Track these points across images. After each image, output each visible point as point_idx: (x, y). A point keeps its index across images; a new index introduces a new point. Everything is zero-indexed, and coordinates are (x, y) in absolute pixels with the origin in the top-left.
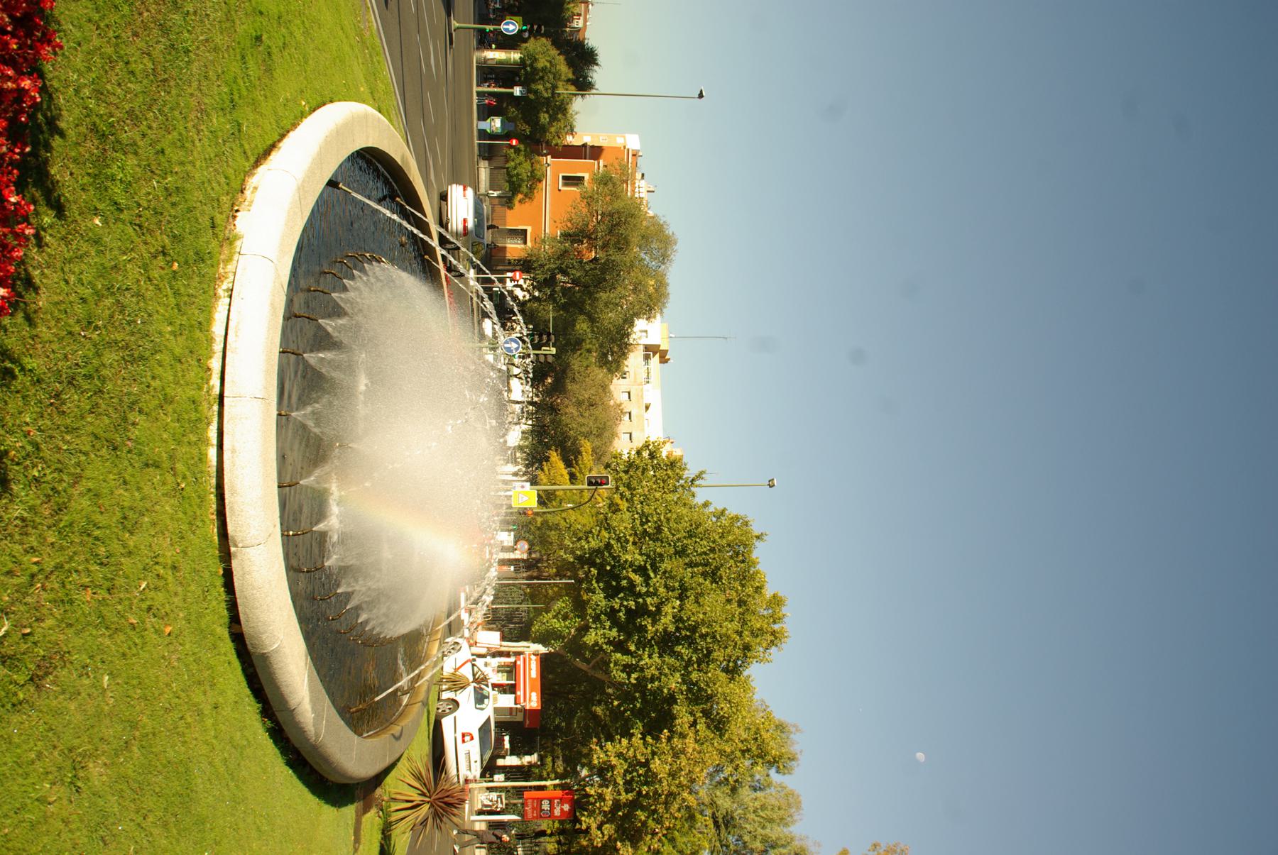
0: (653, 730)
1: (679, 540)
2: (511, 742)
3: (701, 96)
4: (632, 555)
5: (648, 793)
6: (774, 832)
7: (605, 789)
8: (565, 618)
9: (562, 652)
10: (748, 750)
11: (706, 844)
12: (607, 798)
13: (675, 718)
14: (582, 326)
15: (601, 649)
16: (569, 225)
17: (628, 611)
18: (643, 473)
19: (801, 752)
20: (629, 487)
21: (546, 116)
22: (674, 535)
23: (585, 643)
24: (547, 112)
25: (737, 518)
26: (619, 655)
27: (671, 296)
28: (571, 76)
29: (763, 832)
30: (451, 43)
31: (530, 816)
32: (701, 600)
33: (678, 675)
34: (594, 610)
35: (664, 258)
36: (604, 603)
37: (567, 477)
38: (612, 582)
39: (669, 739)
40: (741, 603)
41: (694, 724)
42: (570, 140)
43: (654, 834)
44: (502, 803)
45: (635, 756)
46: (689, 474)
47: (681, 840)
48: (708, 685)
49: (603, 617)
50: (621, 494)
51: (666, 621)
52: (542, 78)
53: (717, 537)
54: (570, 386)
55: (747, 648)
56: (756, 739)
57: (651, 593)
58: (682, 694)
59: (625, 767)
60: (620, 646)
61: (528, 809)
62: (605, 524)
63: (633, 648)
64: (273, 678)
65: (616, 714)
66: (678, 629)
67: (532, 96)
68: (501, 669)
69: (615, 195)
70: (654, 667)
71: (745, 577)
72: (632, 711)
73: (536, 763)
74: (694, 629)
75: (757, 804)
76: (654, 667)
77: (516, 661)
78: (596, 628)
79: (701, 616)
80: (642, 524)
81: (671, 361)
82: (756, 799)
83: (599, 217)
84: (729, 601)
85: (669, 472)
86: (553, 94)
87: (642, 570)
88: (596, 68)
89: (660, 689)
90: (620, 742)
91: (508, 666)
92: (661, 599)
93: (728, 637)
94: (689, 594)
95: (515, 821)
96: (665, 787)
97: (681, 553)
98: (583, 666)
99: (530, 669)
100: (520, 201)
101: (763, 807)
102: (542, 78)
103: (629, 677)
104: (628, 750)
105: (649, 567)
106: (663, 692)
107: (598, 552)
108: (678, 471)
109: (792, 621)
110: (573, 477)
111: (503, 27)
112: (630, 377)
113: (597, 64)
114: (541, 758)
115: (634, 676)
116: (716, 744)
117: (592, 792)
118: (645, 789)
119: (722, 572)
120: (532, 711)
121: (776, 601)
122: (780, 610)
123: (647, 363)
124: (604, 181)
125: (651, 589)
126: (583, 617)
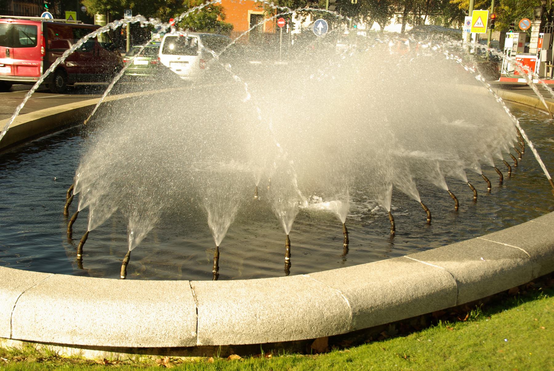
64: (398, 306)
100: (223, 19)
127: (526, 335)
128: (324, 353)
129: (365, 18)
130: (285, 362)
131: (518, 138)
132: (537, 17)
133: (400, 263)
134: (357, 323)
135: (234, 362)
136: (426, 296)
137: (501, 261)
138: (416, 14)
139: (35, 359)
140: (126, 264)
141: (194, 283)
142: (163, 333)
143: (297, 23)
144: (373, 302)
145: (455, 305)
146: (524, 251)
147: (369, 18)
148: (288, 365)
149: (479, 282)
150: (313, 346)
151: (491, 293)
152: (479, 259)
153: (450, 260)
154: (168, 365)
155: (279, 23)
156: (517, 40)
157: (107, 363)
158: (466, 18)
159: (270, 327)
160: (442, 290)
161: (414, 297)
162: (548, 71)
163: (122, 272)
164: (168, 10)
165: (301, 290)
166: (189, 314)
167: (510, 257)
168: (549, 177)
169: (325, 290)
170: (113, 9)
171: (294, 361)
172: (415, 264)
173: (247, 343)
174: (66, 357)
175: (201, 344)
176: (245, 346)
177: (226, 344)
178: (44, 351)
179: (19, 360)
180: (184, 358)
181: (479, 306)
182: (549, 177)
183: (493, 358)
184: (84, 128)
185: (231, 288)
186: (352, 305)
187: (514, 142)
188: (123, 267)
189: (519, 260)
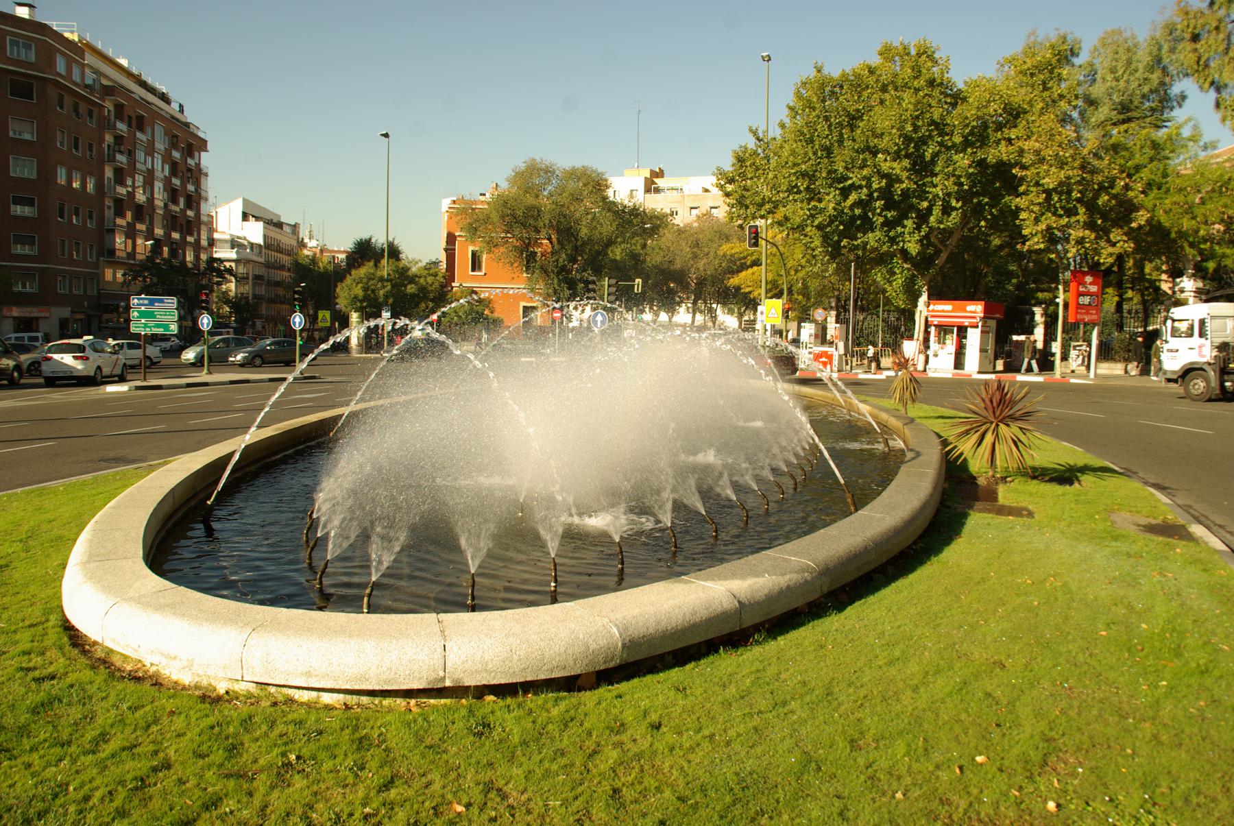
0: (1013, 185)
1: (815, 153)
2: (1019, 334)
3: (386, 135)
4: (830, 202)
5: (1080, 192)
6: (1143, 57)
7: (1071, 237)
8: (892, 273)
9: (928, 278)
10: (1044, 83)
11: (1144, 132)
12: (1081, 235)
13: (1001, 160)
14: (617, 253)
15: (927, 237)
16: (516, 265)
17: (887, 207)
18: (748, 190)
19: (1057, 29)
20: (761, 205)
21: (409, 287)
22: (810, 159)
23: (918, 253)
24: (405, 286)
25: (799, 96)
26: (932, 219)
27: (585, 164)
28: (372, 264)
29: (1141, 70)
30: (314, 377)
31: (1095, 317)
32: (879, 131)
33: (956, 157)
34: (884, 243)
35: (548, 171)
36: (878, 233)
37: (755, 268)
38: (857, 224)
39: (1024, 167)
40: (884, 89)
41: (1009, 141)
42: (444, 266)
43: (1127, 188)
44: (1081, 346)
45: (1039, 204)
46: (751, 143)
47: (1138, 159)
48: (967, 125)
49: (892, 234)
50: (769, 213)
51: (898, 168)
52: (373, 291)
53: (814, 114)
54: (678, 265)
55: (931, 83)
56: (1032, 75)
58: (976, 153)
59: (1050, 215)
60: (923, 217)
61: (1087, 319)
62: (801, 228)
63: (925, 204)
65: (994, 225)
66: (907, 156)
67: (391, 301)
68: (942, 341)
69: (487, 219)
70: (946, 182)
71: (856, 84)
72: (992, 206)
73: (1044, 309)
74: (907, 139)
75: (1109, 77)
76: (946, 182)
77: (935, 325)
78: (904, 242)
79: (894, 131)
80: (799, 192)
81: (661, 166)
82: (1104, 79)
83: (509, 235)
84: (882, 102)
86: (388, 280)
87: (845, 193)
88: (373, 240)
89: (969, 176)
90: (1024, 220)
91: (939, 334)
93: (919, 102)
94: (872, 144)
95: (1100, 334)
96: (1075, 174)
97: (828, 151)
98: (944, 256)
99: (943, 311)
101: (1113, 71)
102: (373, 291)
103: (955, 209)
104: (1032, 211)
106: (972, 174)
107: (826, 238)
109: (908, 36)
110: (757, 263)
111: (297, 327)
112: (675, 207)
113: (370, 239)
114: (1039, 303)
115: (954, 203)
116: (1033, 118)
117: (1074, 250)
118: (1076, 195)
119: (851, 110)
120: (986, 311)
121: (887, 52)
122: (896, 48)
123: (663, 190)
124: (473, 230)
125: (864, 183)
126: (893, 255)
127: (812, 656)
128: (590, 690)
129: (651, 308)
130: (546, 702)
131: (809, 444)
132: (831, 308)
133: (676, 584)
134: (628, 655)
135: (488, 704)
137: (787, 577)
138: (706, 303)
139: (269, 703)
140: (370, 595)
141: (442, 616)
142: (407, 673)
143: (576, 315)
144: (645, 630)
147: (655, 308)
148: (550, 705)
149: (764, 601)
150: (579, 682)
151: (778, 613)
152: (764, 576)
153: (732, 579)
154: (414, 709)
155: (555, 315)
156: (813, 332)
157: (347, 707)
158: (759, 307)
160: (723, 613)
162: (847, 364)
163: (365, 606)
164: (431, 304)
165: (563, 621)
167: (797, 572)
168: (842, 481)
169: (591, 619)
170: (370, 306)
171: (556, 701)
172: (693, 586)
173: (503, 682)
174: (303, 700)
175: (451, 685)
176: (500, 685)
177: (478, 684)
178: (279, 694)
179: (252, 704)
180: (432, 701)
181: (764, 627)
182: (842, 481)
183: (776, 683)
184: (330, 441)
185: (484, 620)
186: (621, 635)
187: (804, 449)
188: (366, 599)
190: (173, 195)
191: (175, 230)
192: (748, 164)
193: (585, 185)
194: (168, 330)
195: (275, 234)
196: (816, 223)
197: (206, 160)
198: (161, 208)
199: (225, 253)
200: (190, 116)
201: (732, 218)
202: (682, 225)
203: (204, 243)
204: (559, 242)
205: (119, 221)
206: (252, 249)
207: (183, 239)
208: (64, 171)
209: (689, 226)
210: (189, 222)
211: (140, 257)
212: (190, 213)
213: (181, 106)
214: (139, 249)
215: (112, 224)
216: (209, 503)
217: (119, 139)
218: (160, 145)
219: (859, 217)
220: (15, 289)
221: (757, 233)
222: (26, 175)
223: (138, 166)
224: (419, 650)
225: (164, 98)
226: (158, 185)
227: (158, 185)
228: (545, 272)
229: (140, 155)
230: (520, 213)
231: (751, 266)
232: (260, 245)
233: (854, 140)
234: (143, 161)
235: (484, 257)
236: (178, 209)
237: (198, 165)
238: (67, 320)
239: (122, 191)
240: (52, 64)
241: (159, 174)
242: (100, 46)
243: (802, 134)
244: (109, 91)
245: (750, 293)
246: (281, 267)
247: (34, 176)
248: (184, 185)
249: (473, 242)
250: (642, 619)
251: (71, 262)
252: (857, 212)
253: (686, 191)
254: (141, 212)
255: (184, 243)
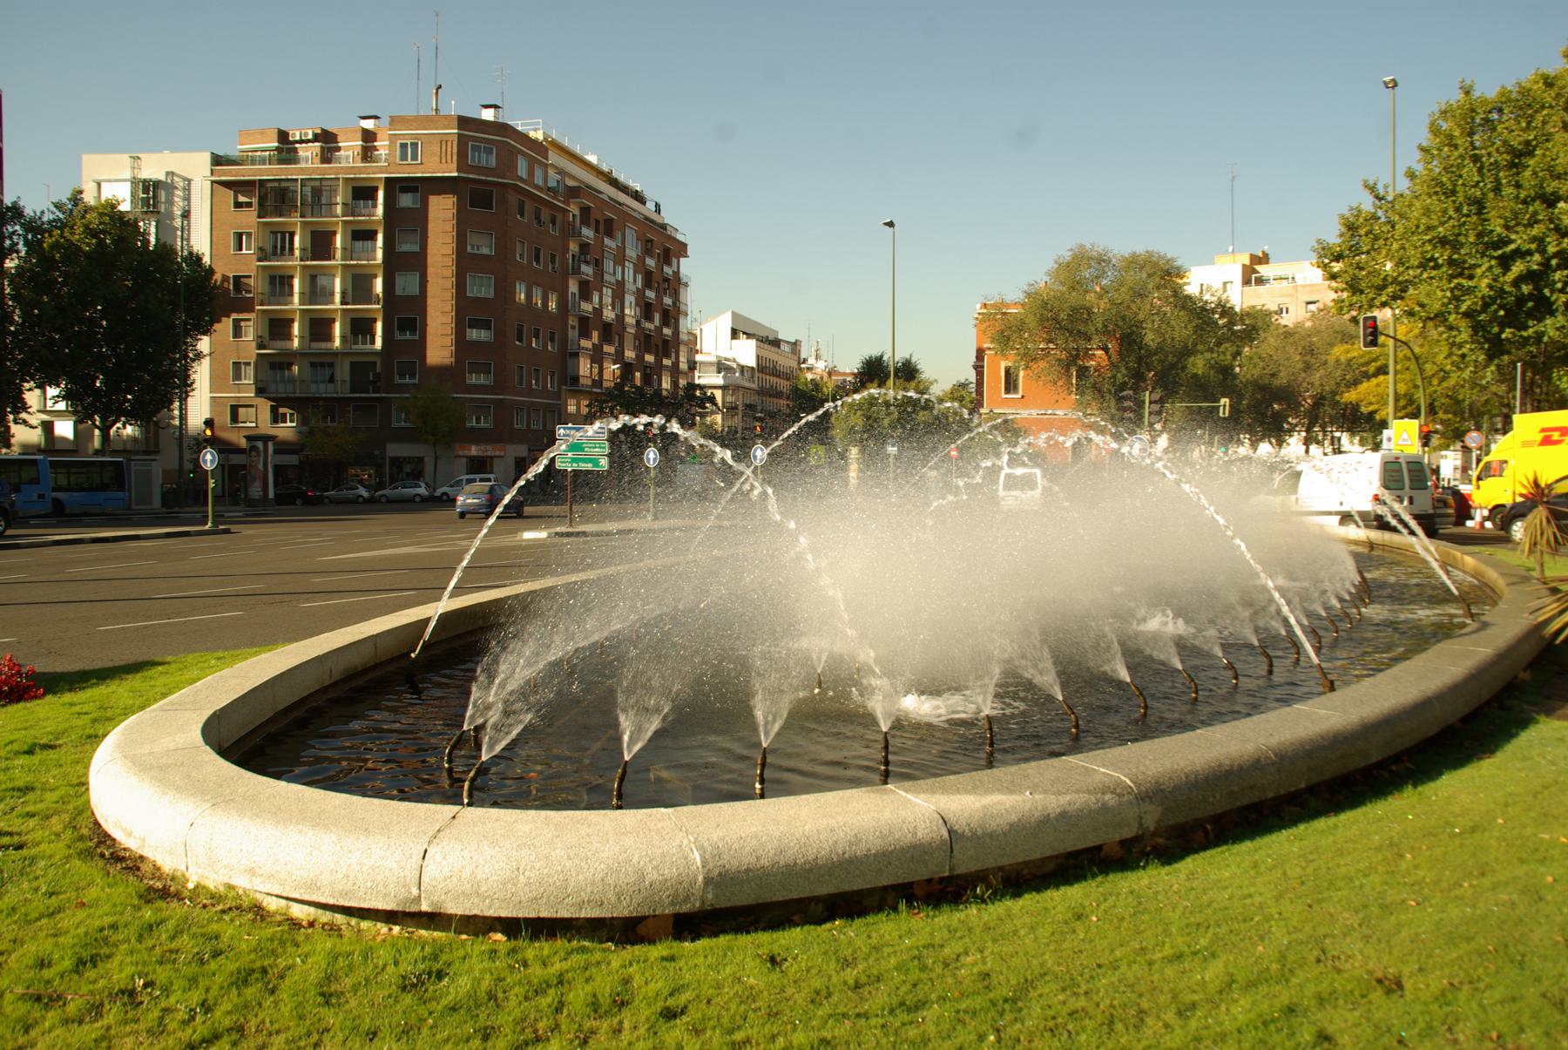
3: (891, 224)
14: (1198, 365)
16: (1060, 383)
25: (1435, 130)
27: (1150, 249)
35: (1102, 260)
37: (1381, 378)
46: (1367, 204)
53: (1456, 154)
57: (1539, 246)
62: (1440, 318)
69: (1021, 327)
80: (1437, 267)
83: (1051, 346)
85: (1362, 232)
87: (1505, 262)
88: (885, 358)
92: (1550, 230)
97: (1479, 204)
105: (1500, 252)
107: (1477, 328)
108: (1361, 220)
110: (1383, 370)
113: (882, 356)
125: (1533, 246)
134: (716, 896)
136: (875, 855)
142: (369, 884)
144: (753, 860)
145: (947, 874)
146: (1128, 781)
149: (1005, 834)
150: (642, 929)
159: (542, 890)
161: (847, 856)
166: (411, 857)
167: (1089, 792)
189: (1108, 797)
190: (647, 310)
191: (649, 352)
192: (1362, 232)
193: (1150, 276)
194: (597, 466)
195: (770, 353)
196: (1464, 308)
197: (686, 267)
198: (632, 326)
199: (708, 379)
200: (668, 217)
201: (1341, 309)
202: (1291, 325)
203: (683, 366)
204: (1120, 353)
205: (585, 343)
206: (742, 372)
207: (658, 361)
208: (539, 293)
209: (1299, 325)
210: (666, 342)
211: (606, 384)
212: (667, 331)
213: (657, 205)
214: (607, 375)
215: (576, 347)
216: (413, 655)
217: (584, 247)
218: (632, 253)
219: (1530, 297)
220: (468, 425)
221: (1375, 327)
222: (483, 295)
223: (606, 277)
224: (388, 854)
225: (638, 197)
226: (630, 299)
227: (630, 299)
228: (1099, 391)
229: (609, 265)
230: (1063, 316)
231: (1375, 375)
232: (752, 368)
233: (1518, 186)
234: (611, 271)
235: (1022, 374)
236: (652, 327)
237: (677, 274)
238: (523, 459)
239: (587, 307)
240: (513, 166)
241: (630, 286)
242: (566, 143)
243: (1442, 184)
244: (574, 193)
245: (1375, 412)
246: (778, 395)
247: (491, 295)
248: (659, 298)
249: (1005, 357)
250: (754, 842)
251: (530, 392)
252: (1526, 289)
253: (1299, 281)
254: (610, 332)
255: (659, 367)
